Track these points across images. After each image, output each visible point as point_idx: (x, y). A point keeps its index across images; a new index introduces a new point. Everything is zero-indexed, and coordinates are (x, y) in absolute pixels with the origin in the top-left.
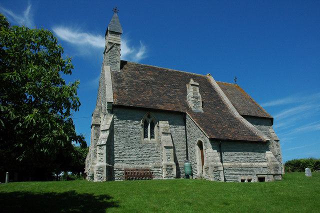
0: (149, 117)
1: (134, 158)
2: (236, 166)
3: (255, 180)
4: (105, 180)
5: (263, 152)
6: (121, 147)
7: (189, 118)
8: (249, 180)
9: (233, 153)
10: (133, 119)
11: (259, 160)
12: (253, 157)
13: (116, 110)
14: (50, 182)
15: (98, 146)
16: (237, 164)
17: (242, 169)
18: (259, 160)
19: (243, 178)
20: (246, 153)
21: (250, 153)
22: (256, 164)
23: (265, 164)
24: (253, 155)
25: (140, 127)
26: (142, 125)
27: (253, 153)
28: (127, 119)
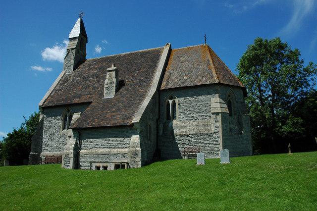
0: (69, 111)
1: (54, 146)
2: (92, 153)
3: (111, 167)
4: (140, 166)
5: (128, 137)
6: (46, 139)
7: (167, 84)
8: (105, 168)
9: (93, 140)
10: (56, 116)
11: (121, 146)
12: (114, 144)
13: (45, 111)
14: (21, 166)
15: (180, 106)
16: (94, 151)
17: (98, 155)
18: (121, 146)
19: (98, 165)
20: (107, 139)
21: (111, 139)
22: (116, 151)
23: (126, 150)
24: (114, 141)
25: (60, 121)
26: (62, 119)
27: (115, 139)
28: (52, 117)
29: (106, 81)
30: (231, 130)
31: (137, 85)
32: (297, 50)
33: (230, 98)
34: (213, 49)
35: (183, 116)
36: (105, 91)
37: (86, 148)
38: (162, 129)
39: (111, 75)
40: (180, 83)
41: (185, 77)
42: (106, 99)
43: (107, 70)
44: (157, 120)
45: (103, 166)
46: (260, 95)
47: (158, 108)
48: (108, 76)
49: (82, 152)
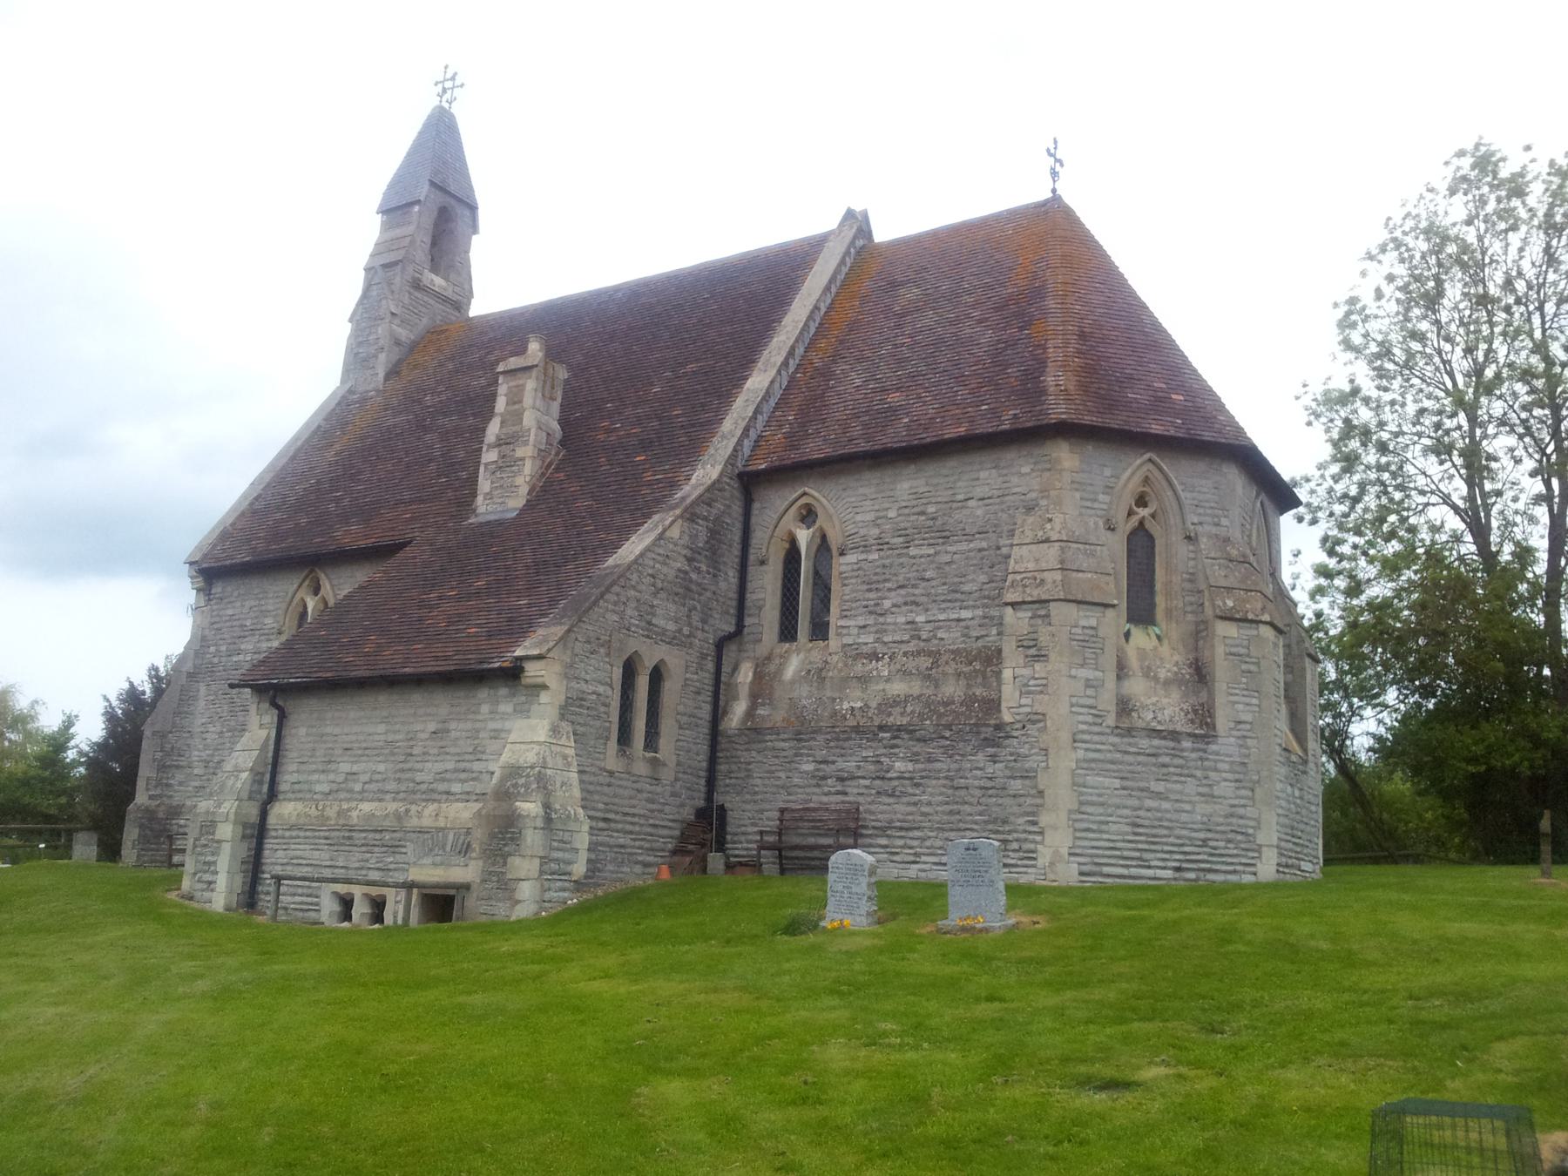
29: (493, 429)
30: (1125, 707)
31: (645, 445)
32: (850, 215)
33: (1143, 512)
34: (1403, 216)
35: (861, 621)
36: (484, 485)
37: (298, 795)
38: (744, 692)
39: (515, 398)
40: (856, 430)
41: (895, 398)
42: (1304, 669)
43: (500, 368)
44: (720, 645)
45: (366, 895)
46: (1470, 498)
47: (732, 575)
48: (501, 404)
49: (285, 810)
